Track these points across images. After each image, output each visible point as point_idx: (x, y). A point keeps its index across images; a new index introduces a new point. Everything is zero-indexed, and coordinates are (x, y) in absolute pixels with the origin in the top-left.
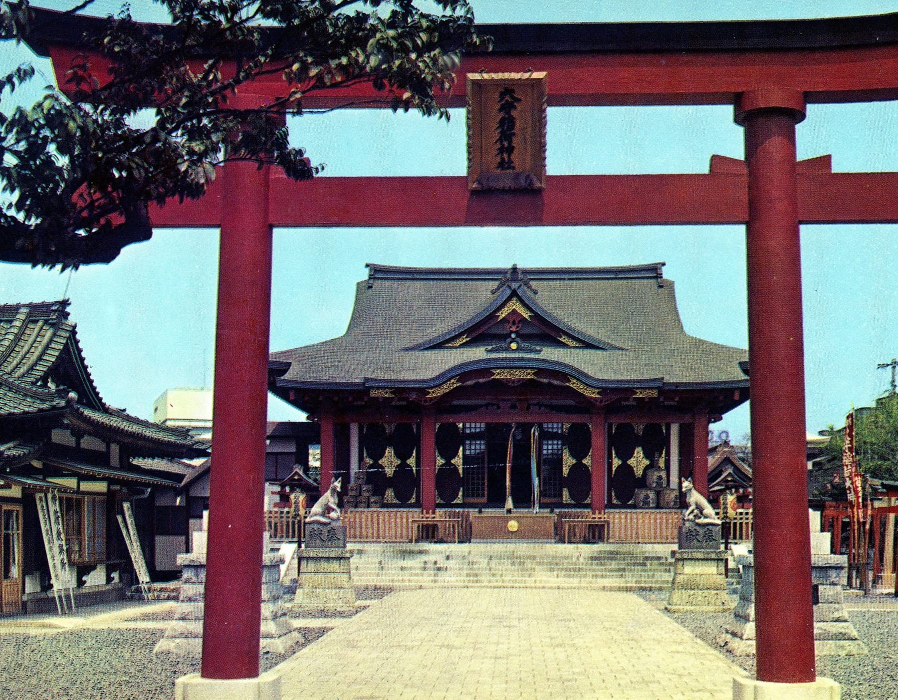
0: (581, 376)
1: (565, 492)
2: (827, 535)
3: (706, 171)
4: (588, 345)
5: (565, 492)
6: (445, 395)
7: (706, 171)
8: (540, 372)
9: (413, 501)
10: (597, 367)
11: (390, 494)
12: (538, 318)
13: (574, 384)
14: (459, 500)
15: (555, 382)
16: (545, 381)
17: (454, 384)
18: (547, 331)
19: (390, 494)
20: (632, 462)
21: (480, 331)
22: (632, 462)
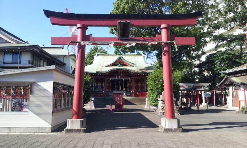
21: (114, 64)
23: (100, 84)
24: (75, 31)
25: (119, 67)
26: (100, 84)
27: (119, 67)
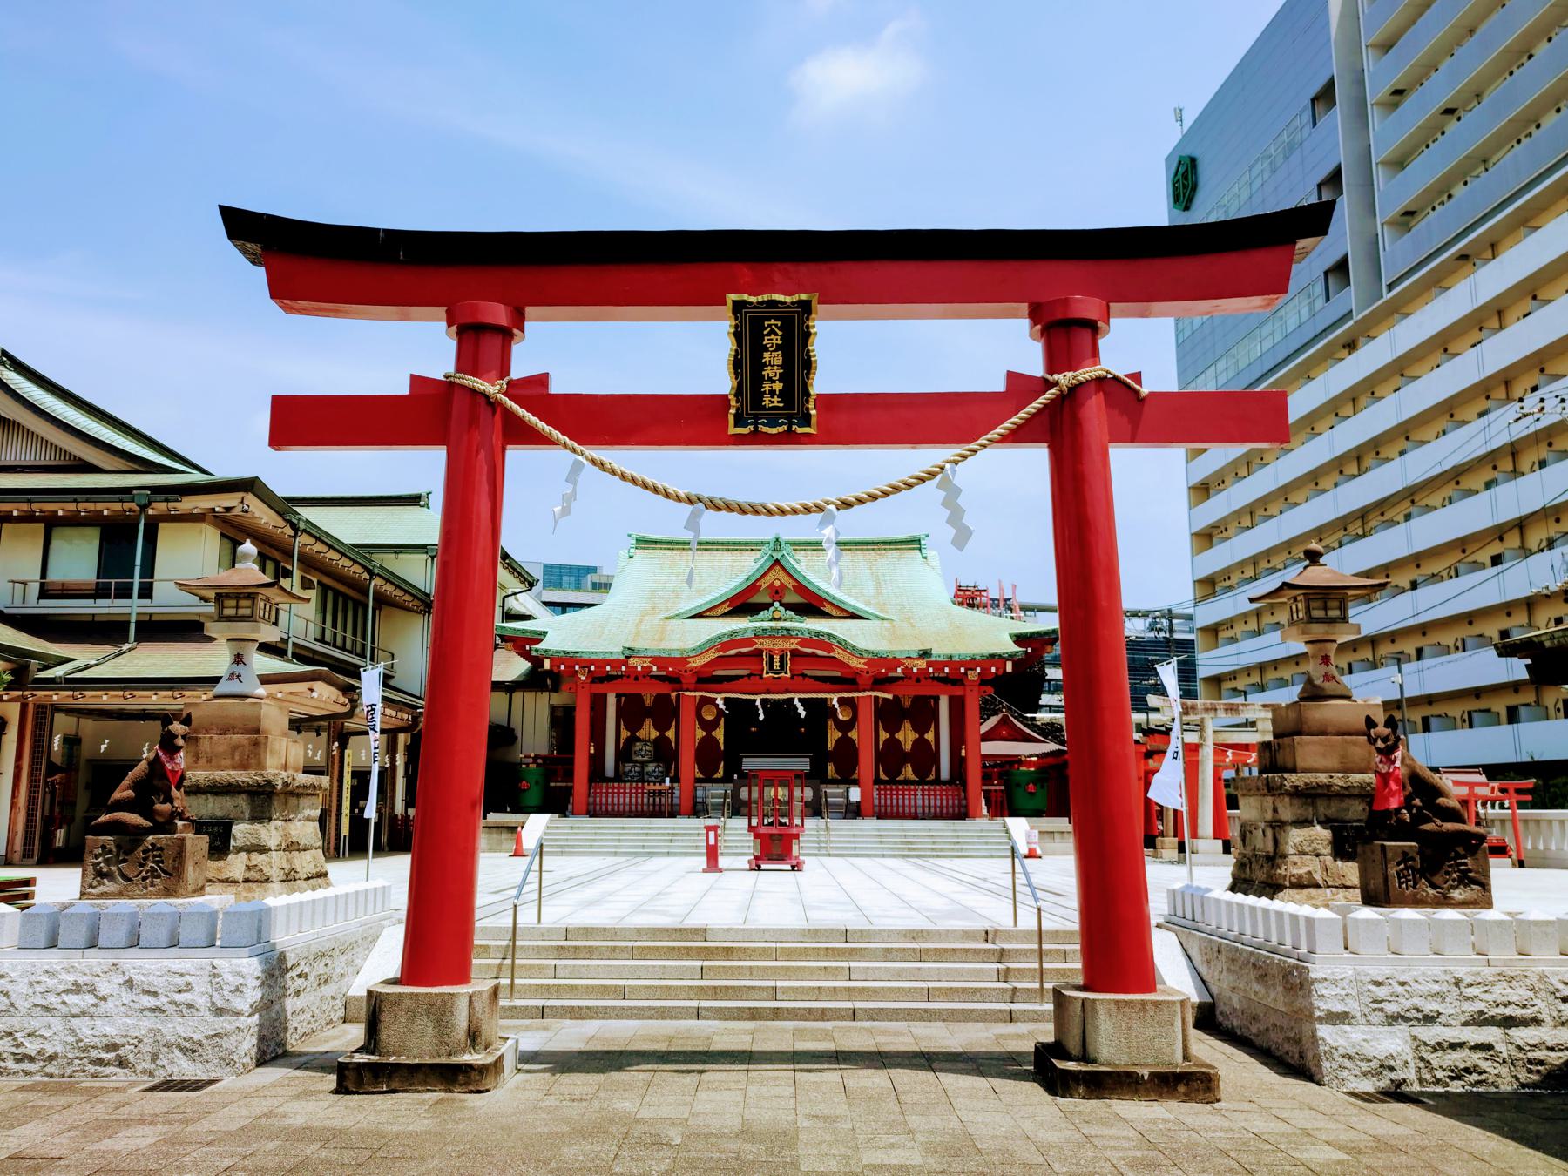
0: (844, 645)
1: (831, 767)
2: (366, 816)
3: (406, 391)
4: (854, 616)
5: (831, 767)
6: (706, 665)
7: (406, 391)
8: (805, 642)
9: (932, 777)
10: (862, 638)
11: (908, 772)
12: (801, 588)
13: (838, 654)
14: (720, 774)
15: (744, 650)
16: (809, 651)
17: (712, 656)
18: (812, 605)
19: (908, 772)
20: (900, 736)
21: (741, 605)
22: (900, 736)
23: (654, 734)
24: (399, 349)
25: (773, 624)
26: (654, 734)
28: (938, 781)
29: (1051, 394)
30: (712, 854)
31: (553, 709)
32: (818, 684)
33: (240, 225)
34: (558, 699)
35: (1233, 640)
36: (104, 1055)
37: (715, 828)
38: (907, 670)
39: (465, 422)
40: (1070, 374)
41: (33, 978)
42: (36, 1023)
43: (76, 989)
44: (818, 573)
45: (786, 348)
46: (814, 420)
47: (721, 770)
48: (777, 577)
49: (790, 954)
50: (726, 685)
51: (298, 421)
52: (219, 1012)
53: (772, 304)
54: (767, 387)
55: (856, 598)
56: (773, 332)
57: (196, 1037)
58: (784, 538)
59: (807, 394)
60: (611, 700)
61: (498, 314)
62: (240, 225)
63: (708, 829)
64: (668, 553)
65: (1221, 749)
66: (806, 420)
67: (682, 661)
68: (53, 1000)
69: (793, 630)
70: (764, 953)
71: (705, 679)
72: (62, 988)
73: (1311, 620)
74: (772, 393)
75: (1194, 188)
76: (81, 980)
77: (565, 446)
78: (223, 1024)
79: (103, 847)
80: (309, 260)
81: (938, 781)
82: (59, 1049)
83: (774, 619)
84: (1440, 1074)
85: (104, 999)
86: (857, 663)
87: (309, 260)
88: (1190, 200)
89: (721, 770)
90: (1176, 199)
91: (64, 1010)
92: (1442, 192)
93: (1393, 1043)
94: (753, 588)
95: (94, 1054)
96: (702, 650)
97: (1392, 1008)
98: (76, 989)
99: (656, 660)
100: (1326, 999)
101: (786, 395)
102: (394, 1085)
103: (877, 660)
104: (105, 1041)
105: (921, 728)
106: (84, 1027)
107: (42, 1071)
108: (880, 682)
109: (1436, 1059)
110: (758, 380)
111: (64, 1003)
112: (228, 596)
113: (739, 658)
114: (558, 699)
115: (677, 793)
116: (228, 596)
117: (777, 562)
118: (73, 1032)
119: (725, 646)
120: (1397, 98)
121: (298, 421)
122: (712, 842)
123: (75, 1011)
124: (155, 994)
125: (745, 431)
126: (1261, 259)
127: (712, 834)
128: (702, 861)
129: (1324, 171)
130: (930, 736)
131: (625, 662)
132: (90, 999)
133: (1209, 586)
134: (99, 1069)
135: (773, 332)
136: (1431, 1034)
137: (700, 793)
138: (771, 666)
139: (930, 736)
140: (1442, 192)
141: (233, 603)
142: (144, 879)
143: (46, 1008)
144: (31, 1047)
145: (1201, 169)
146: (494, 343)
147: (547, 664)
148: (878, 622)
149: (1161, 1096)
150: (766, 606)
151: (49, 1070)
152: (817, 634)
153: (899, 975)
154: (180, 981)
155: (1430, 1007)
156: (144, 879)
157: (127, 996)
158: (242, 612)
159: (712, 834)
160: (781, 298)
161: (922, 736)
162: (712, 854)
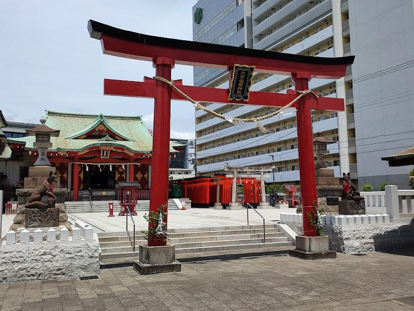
0: (128, 149)
13: (126, 151)
18: (114, 136)
21: (89, 135)
24: (140, 69)
25: (106, 142)
27: (106, 142)
28: (148, 189)
29: (301, 95)
30: (111, 211)
31: (21, 168)
32: (119, 161)
33: (97, 28)
34: (22, 164)
35: (206, 149)
36: (57, 272)
37: (112, 204)
38: (146, 157)
39: (162, 92)
40: (305, 91)
41: (30, 252)
42: (33, 265)
43: (45, 254)
44: (113, 125)
45: (245, 79)
46: (248, 98)
47: (82, 186)
48: (102, 127)
49: (199, 234)
50: (88, 160)
51: (113, 87)
52: (91, 257)
53: (245, 67)
54: (239, 88)
55: (121, 132)
56: (243, 75)
57: (85, 264)
58: (103, 115)
59: (248, 91)
60: (111, 166)
61: (167, 61)
62: (97, 28)
63: (110, 204)
64: (60, 117)
65: (238, 179)
66: (246, 98)
67: (76, 153)
68: (38, 257)
69: (113, 144)
70: (192, 235)
71: (82, 158)
72: (40, 254)
73: (320, 149)
74: (240, 90)
75: (201, 18)
76: (47, 251)
77: (190, 101)
78: (91, 261)
79: (33, 212)
80: (116, 40)
81: (148, 189)
82: (42, 272)
83: (106, 140)
84: (365, 249)
85: (54, 256)
86: (131, 154)
87: (116, 40)
88: (200, 21)
89: (82, 186)
90: (196, 20)
91: (42, 260)
92: (269, 31)
93: (357, 244)
94: (93, 130)
95: (54, 272)
96: (83, 149)
97: (357, 236)
98: (45, 254)
99: (68, 152)
100: (345, 236)
101: (243, 91)
102: (158, 271)
103: (138, 154)
104: (57, 268)
105: (143, 174)
106: (48, 264)
107: (37, 279)
108: (137, 160)
109: (365, 246)
110: (237, 86)
111: (42, 258)
112: (40, 134)
113: (94, 152)
114: (22, 164)
115: (72, 194)
116: (40, 134)
117: (102, 123)
118: (46, 266)
119: (90, 148)
120: (259, 2)
121: (113, 87)
122: (111, 208)
123: (46, 260)
124: (71, 254)
125: (232, 99)
126: (341, 66)
127: (111, 206)
128: (108, 214)
129: (239, 19)
130: (146, 176)
131: (57, 153)
132: (50, 256)
133: (200, 133)
134: (56, 276)
135: (243, 75)
136: (364, 241)
137: (80, 193)
138: (107, 153)
139: (146, 176)
140: (269, 31)
141: (42, 136)
142: (47, 221)
143: (37, 260)
144: (33, 272)
145: (203, 12)
146: (166, 68)
147: (30, 153)
148: (132, 142)
149: (327, 258)
150: (104, 136)
151: (39, 278)
152: (120, 145)
153: (228, 238)
154: (78, 249)
155: (363, 235)
156: (47, 221)
157: (62, 255)
158: (45, 139)
159: (111, 206)
160: (247, 66)
161: (143, 175)
162: (111, 211)
